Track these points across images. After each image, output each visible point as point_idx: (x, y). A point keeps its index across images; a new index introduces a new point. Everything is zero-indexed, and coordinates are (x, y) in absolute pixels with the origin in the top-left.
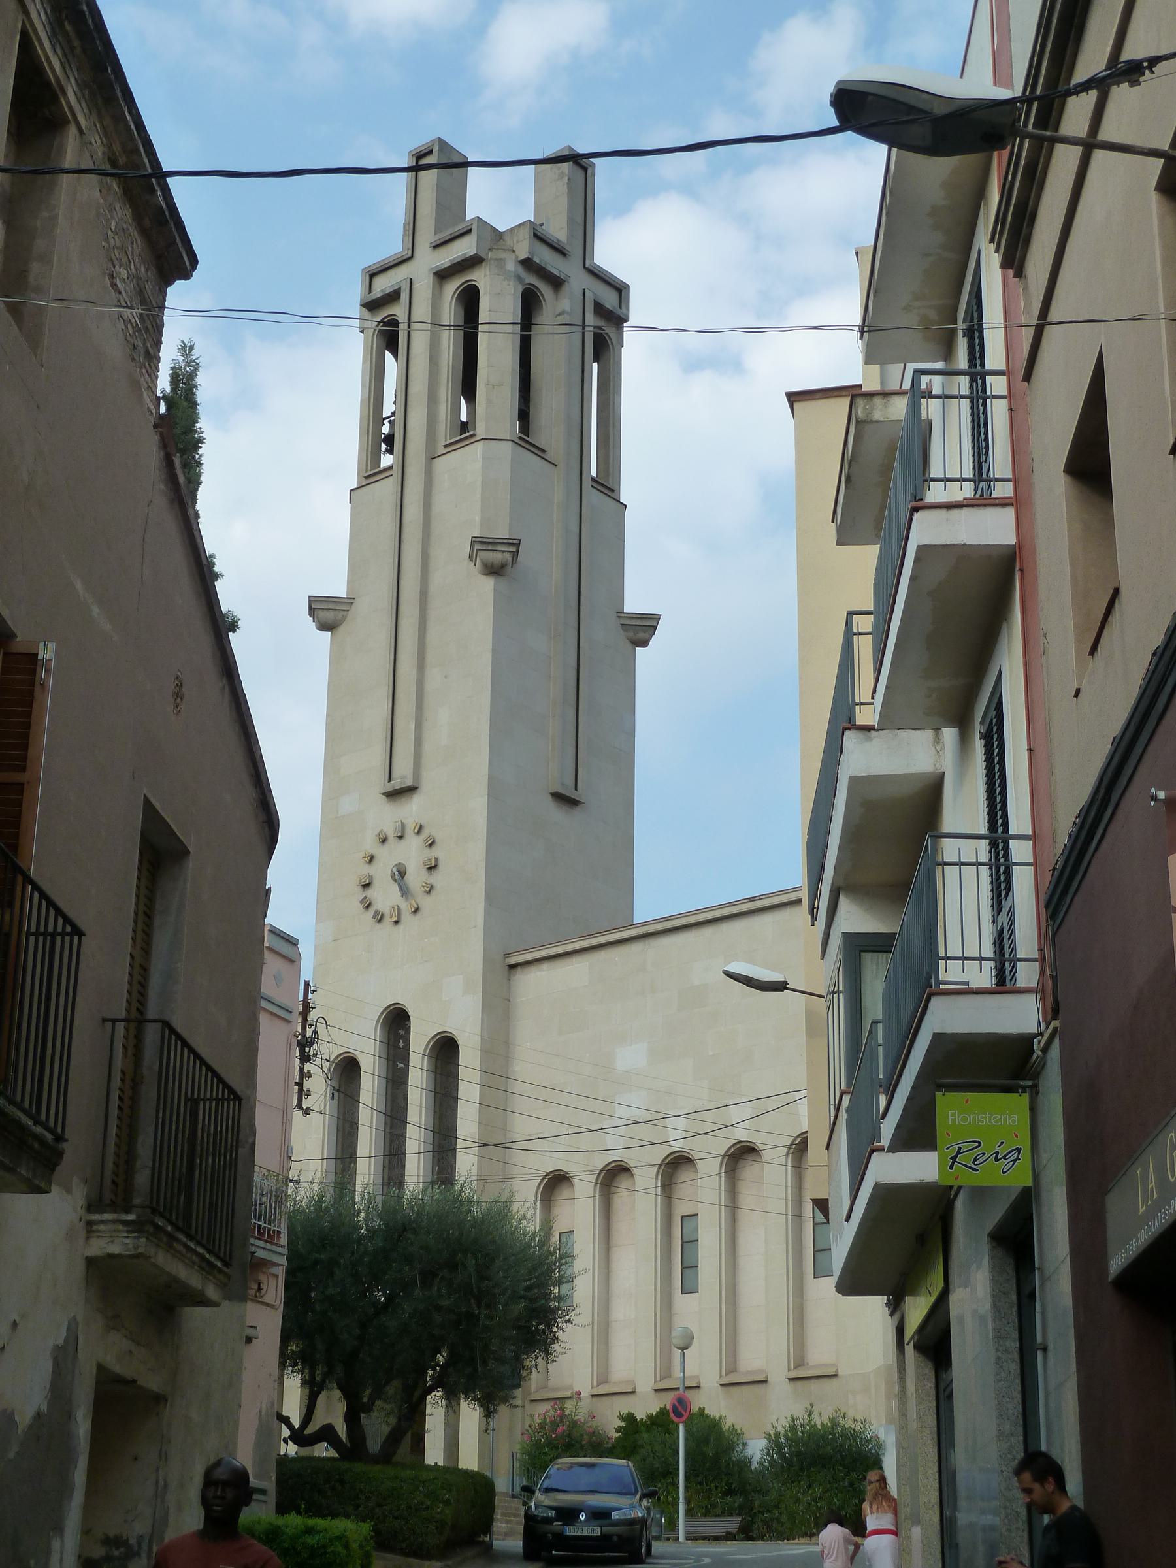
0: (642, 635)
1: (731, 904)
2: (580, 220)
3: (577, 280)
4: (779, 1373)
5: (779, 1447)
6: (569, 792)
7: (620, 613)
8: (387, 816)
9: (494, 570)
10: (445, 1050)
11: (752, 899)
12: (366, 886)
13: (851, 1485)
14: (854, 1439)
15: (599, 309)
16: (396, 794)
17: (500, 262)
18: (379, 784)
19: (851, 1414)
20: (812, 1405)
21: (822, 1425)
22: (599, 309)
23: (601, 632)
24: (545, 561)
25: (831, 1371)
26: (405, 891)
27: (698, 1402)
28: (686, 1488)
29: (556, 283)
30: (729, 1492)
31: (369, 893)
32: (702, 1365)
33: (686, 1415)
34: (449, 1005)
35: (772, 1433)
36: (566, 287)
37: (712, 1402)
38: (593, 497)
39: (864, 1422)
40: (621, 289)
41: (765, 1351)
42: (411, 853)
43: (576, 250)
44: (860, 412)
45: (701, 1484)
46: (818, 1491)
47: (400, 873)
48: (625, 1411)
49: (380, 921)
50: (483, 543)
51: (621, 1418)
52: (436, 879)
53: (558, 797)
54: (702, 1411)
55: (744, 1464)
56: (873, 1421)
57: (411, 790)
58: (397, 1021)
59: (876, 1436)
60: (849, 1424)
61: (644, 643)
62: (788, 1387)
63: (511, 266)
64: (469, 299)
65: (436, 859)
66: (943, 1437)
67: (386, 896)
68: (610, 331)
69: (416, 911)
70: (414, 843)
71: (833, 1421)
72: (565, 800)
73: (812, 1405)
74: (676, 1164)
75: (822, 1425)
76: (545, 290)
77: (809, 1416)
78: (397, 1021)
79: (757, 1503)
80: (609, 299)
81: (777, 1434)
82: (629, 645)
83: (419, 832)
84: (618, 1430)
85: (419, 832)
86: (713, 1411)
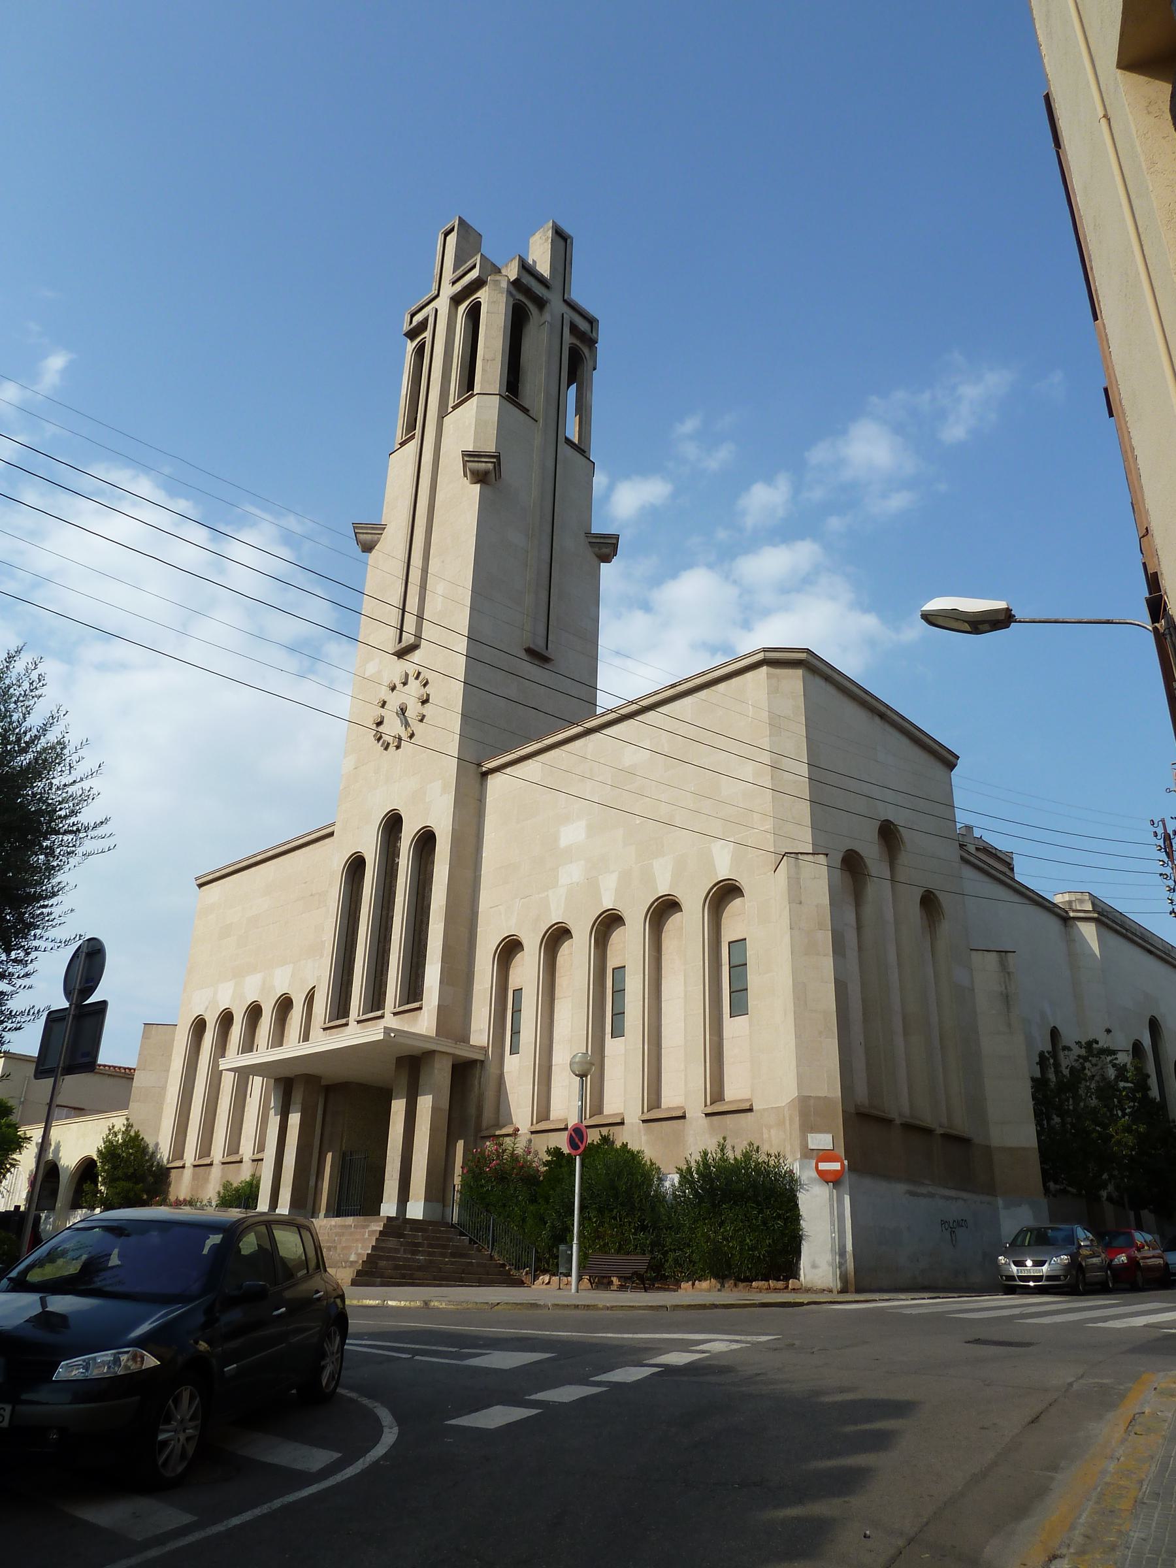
0: (605, 550)
1: (656, 693)
2: (561, 270)
3: (556, 305)
4: (696, 1110)
5: (692, 1183)
6: (539, 645)
7: (588, 534)
8: (396, 669)
9: (480, 478)
10: (426, 840)
11: (673, 686)
12: (379, 724)
13: (764, 1223)
14: (768, 1174)
15: (574, 328)
16: (402, 654)
17: (497, 282)
18: (392, 646)
19: (765, 1148)
20: (725, 1139)
21: (735, 1159)
22: (574, 328)
23: (570, 543)
24: (524, 476)
25: (746, 1106)
26: (407, 724)
27: (621, 1137)
28: (580, 1224)
29: (541, 304)
30: (643, 1228)
31: (381, 729)
32: (622, 1096)
33: (582, 1147)
34: (433, 808)
35: (685, 1167)
36: (548, 308)
37: (634, 1137)
38: (564, 449)
39: (778, 1156)
40: (592, 322)
41: (683, 1086)
42: (410, 694)
43: (557, 285)
44: (853, 1289)
45: (615, 1219)
46: (729, 1228)
47: (403, 710)
48: (552, 1146)
49: (386, 749)
50: (469, 456)
51: (548, 1152)
52: (428, 710)
53: (530, 651)
54: (625, 1146)
55: (660, 1198)
56: (788, 1156)
57: (414, 647)
58: (393, 824)
59: (791, 1171)
60: (762, 1158)
61: (607, 559)
62: (705, 1121)
63: (504, 285)
64: (474, 313)
65: (428, 695)
66: (693, 1314)
67: (393, 727)
68: (586, 351)
69: (412, 736)
70: (414, 686)
71: (747, 1156)
72: (538, 656)
73: (725, 1139)
74: (609, 922)
75: (735, 1159)
76: (532, 308)
77: (722, 1150)
78: (393, 824)
79: (669, 1240)
80: (583, 326)
81: (689, 1169)
82: (596, 559)
83: (417, 678)
84: (546, 1164)
85: (417, 678)
86: (634, 1146)
